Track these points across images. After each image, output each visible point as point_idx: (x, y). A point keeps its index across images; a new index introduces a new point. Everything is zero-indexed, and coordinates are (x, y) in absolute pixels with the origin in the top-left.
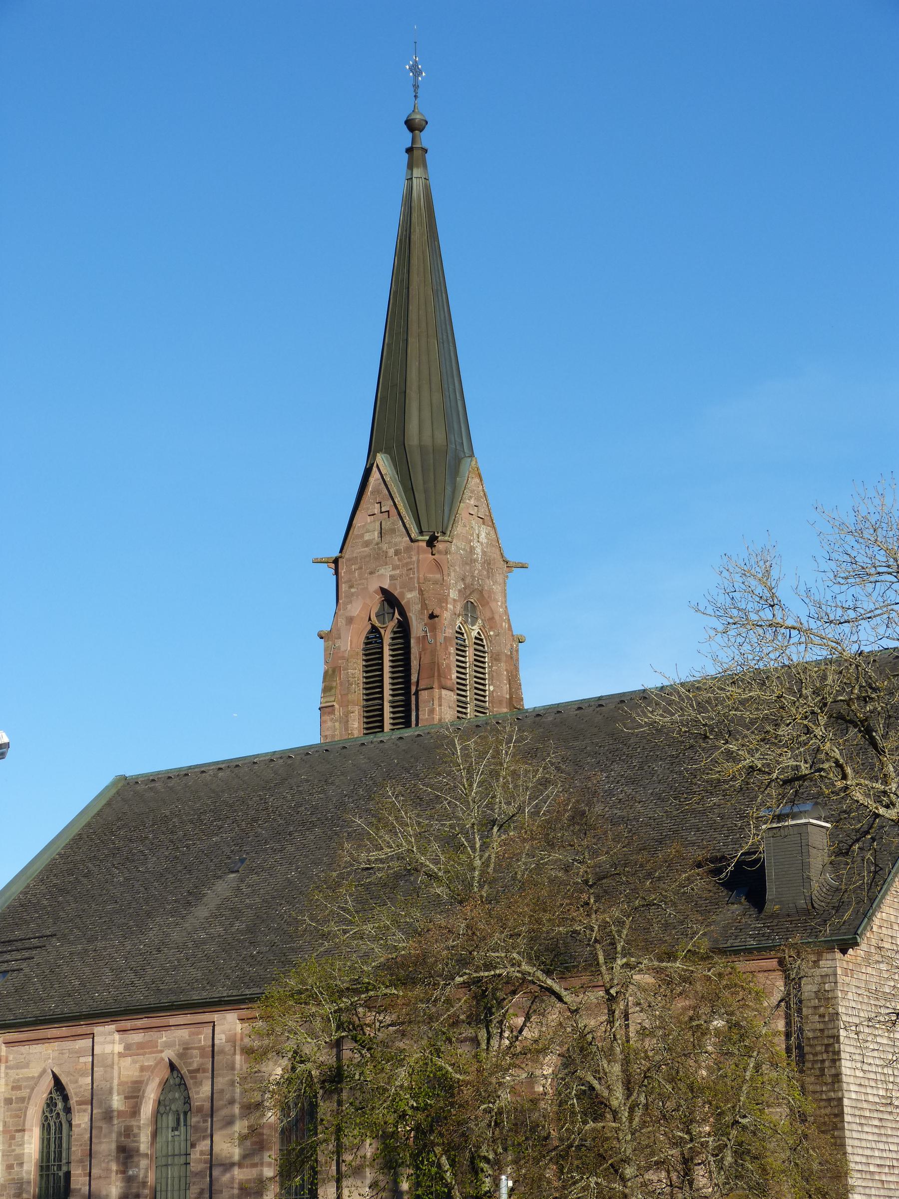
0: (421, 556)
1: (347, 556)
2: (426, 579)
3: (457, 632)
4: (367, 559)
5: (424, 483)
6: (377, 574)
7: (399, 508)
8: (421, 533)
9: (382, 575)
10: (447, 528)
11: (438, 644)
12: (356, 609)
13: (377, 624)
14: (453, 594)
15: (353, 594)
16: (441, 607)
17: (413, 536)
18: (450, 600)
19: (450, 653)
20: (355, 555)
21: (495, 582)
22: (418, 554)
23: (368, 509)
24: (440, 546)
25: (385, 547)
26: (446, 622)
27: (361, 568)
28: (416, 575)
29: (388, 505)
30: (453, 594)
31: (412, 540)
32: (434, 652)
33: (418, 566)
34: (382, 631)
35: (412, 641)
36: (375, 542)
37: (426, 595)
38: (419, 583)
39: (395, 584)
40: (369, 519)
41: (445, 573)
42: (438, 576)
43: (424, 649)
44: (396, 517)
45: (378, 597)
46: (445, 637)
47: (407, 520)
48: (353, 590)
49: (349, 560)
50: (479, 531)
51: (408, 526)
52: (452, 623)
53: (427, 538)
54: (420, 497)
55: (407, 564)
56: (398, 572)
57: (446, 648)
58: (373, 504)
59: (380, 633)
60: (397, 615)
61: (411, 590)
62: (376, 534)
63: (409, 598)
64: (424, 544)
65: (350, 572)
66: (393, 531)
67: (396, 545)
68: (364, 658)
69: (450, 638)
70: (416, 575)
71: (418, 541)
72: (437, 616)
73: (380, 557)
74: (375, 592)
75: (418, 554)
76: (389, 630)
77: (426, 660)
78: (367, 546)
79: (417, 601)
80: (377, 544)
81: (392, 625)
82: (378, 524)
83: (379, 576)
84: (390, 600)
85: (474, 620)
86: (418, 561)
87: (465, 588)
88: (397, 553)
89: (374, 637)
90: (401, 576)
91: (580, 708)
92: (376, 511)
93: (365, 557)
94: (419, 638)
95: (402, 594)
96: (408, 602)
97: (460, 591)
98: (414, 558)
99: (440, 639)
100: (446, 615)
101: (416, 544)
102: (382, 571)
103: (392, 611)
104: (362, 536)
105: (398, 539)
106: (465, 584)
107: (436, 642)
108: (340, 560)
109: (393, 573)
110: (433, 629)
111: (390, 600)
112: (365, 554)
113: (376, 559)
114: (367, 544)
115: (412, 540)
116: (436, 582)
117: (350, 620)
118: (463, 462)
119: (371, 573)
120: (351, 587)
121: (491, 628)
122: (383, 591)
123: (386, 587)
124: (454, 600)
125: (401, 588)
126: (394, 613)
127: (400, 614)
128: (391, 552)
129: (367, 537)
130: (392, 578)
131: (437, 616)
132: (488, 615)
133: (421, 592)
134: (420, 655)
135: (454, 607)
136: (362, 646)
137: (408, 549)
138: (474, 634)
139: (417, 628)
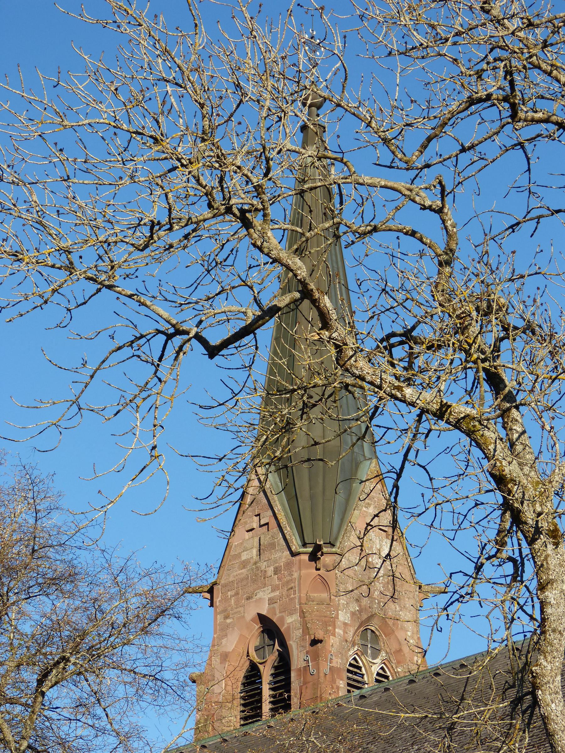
0: (303, 572)
1: (223, 582)
2: (308, 599)
3: (351, 665)
4: (244, 583)
5: (311, 489)
6: (255, 598)
7: (279, 517)
8: (304, 545)
9: (260, 599)
10: (336, 539)
11: (322, 675)
12: (231, 643)
13: (256, 660)
14: (343, 617)
15: (228, 626)
16: (327, 631)
17: (293, 548)
18: (338, 623)
19: (338, 688)
20: (231, 579)
21: (403, 608)
22: (300, 569)
23: (246, 523)
24: (326, 560)
25: (263, 565)
26: (333, 650)
27: (237, 594)
28: (297, 594)
29: (267, 517)
30: (343, 617)
31: (293, 554)
32: (316, 685)
33: (299, 584)
34: (261, 667)
35: (293, 674)
36: (252, 561)
37: (308, 617)
38: (300, 604)
39: (274, 608)
40: (247, 535)
41: (333, 591)
42: (325, 595)
43: (305, 683)
44: (276, 530)
45: (257, 627)
46: (331, 668)
47: (288, 530)
48: (228, 621)
49: (225, 586)
50: (381, 545)
51: (288, 537)
52: (342, 653)
53: (310, 550)
54: (305, 505)
55: (288, 582)
56: (277, 593)
57: (333, 681)
58: (250, 517)
59: (259, 671)
60: (277, 646)
61: (291, 614)
62: (255, 552)
63: (289, 623)
64: (306, 557)
65: (226, 599)
66: (272, 546)
67: (275, 561)
68: (242, 702)
69: (339, 670)
70: (297, 594)
71: (299, 554)
72: (321, 641)
73: (257, 578)
74: (253, 620)
75: (300, 569)
76: (269, 665)
77: (308, 694)
78: (244, 567)
79: (298, 625)
80: (255, 563)
81: (272, 658)
82: (256, 540)
83: (256, 601)
84: (270, 629)
85: (376, 652)
86: (300, 577)
87: (360, 611)
88: (277, 571)
89: (253, 675)
90: (281, 597)
91: (412, 682)
92: (255, 525)
93: (242, 580)
94: (299, 670)
95: (282, 619)
96: (289, 628)
97: (353, 614)
98: (296, 575)
99: (325, 668)
100: (333, 642)
101: (298, 558)
102: (261, 594)
103: (272, 643)
104: (239, 556)
105: (278, 555)
106: (360, 606)
107: (318, 672)
108: (215, 587)
109: (273, 595)
110: (316, 657)
111: (270, 629)
112: (242, 576)
113: (254, 581)
114: (244, 564)
115: (293, 554)
116: (321, 602)
117: (225, 657)
118: (362, 466)
119: (248, 598)
120: (226, 617)
121: (398, 663)
122: (263, 619)
123: (264, 613)
124: (345, 624)
125: (280, 612)
126: (274, 645)
127: (279, 646)
128: (270, 571)
129: (244, 556)
130: (272, 601)
131: (321, 641)
132: (394, 646)
133: (303, 614)
134: (301, 688)
135: (345, 632)
136: (240, 687)
137: (288, 565)
138: (375, 669)
139: (298, 658)
